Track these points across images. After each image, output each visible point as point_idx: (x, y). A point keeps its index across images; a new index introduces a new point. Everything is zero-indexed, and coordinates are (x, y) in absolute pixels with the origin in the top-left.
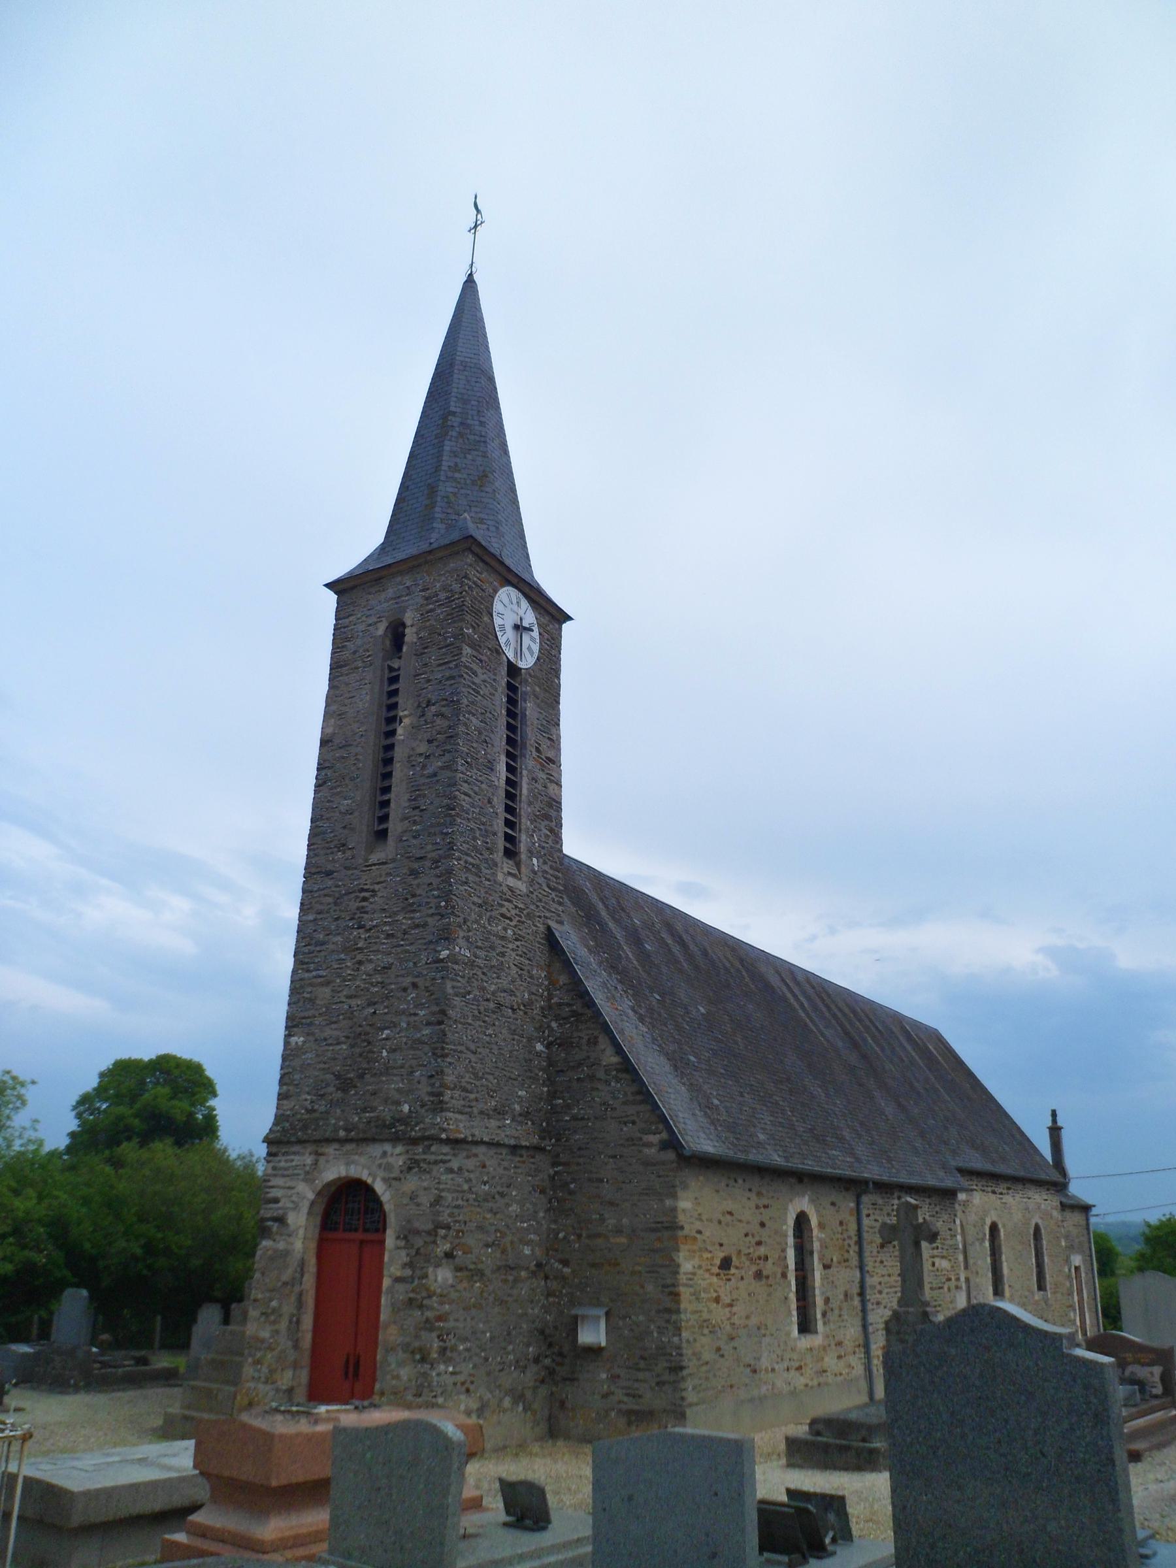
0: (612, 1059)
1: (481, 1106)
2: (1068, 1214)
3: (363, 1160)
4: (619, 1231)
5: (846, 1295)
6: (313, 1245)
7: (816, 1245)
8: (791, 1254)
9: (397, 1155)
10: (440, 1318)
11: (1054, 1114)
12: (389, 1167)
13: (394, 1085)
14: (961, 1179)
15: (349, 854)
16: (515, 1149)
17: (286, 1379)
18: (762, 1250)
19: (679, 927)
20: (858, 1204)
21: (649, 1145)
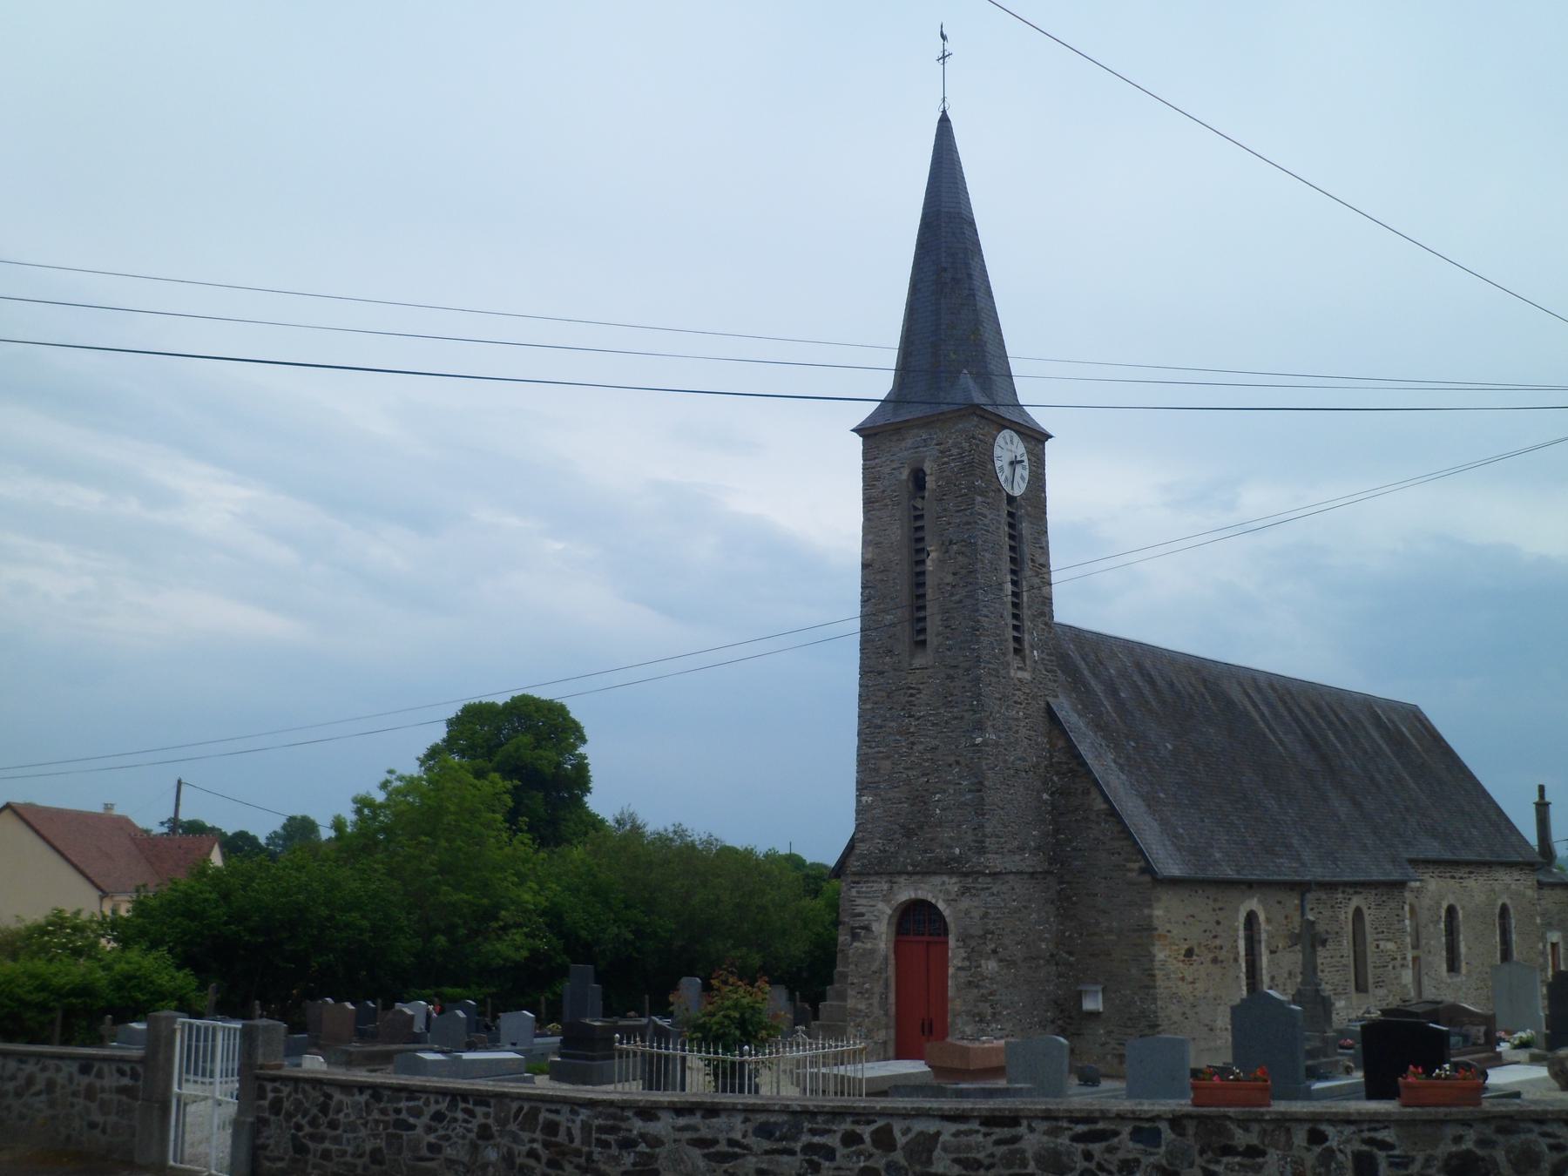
0: (1100, 805)
1: (1008, 846)
2: (1546, 892)
3: (927, 887)
4: (1110, 931)
5: (1290, 974)
6: (892, 945)
7: (1264, 936)
8: (1242, 944)
9: (953, 885)
10: (991, 994)
11: (1542, 789)
12: (948, 892)
13: (947, 834)
14: (1411, 870)
15: (895, 659)
16: (1032, 874)
17: (881, 1035)
18: (1218, 942)
19: (1148, 664)
20: (1302, 901)
21: (1131, 870)
